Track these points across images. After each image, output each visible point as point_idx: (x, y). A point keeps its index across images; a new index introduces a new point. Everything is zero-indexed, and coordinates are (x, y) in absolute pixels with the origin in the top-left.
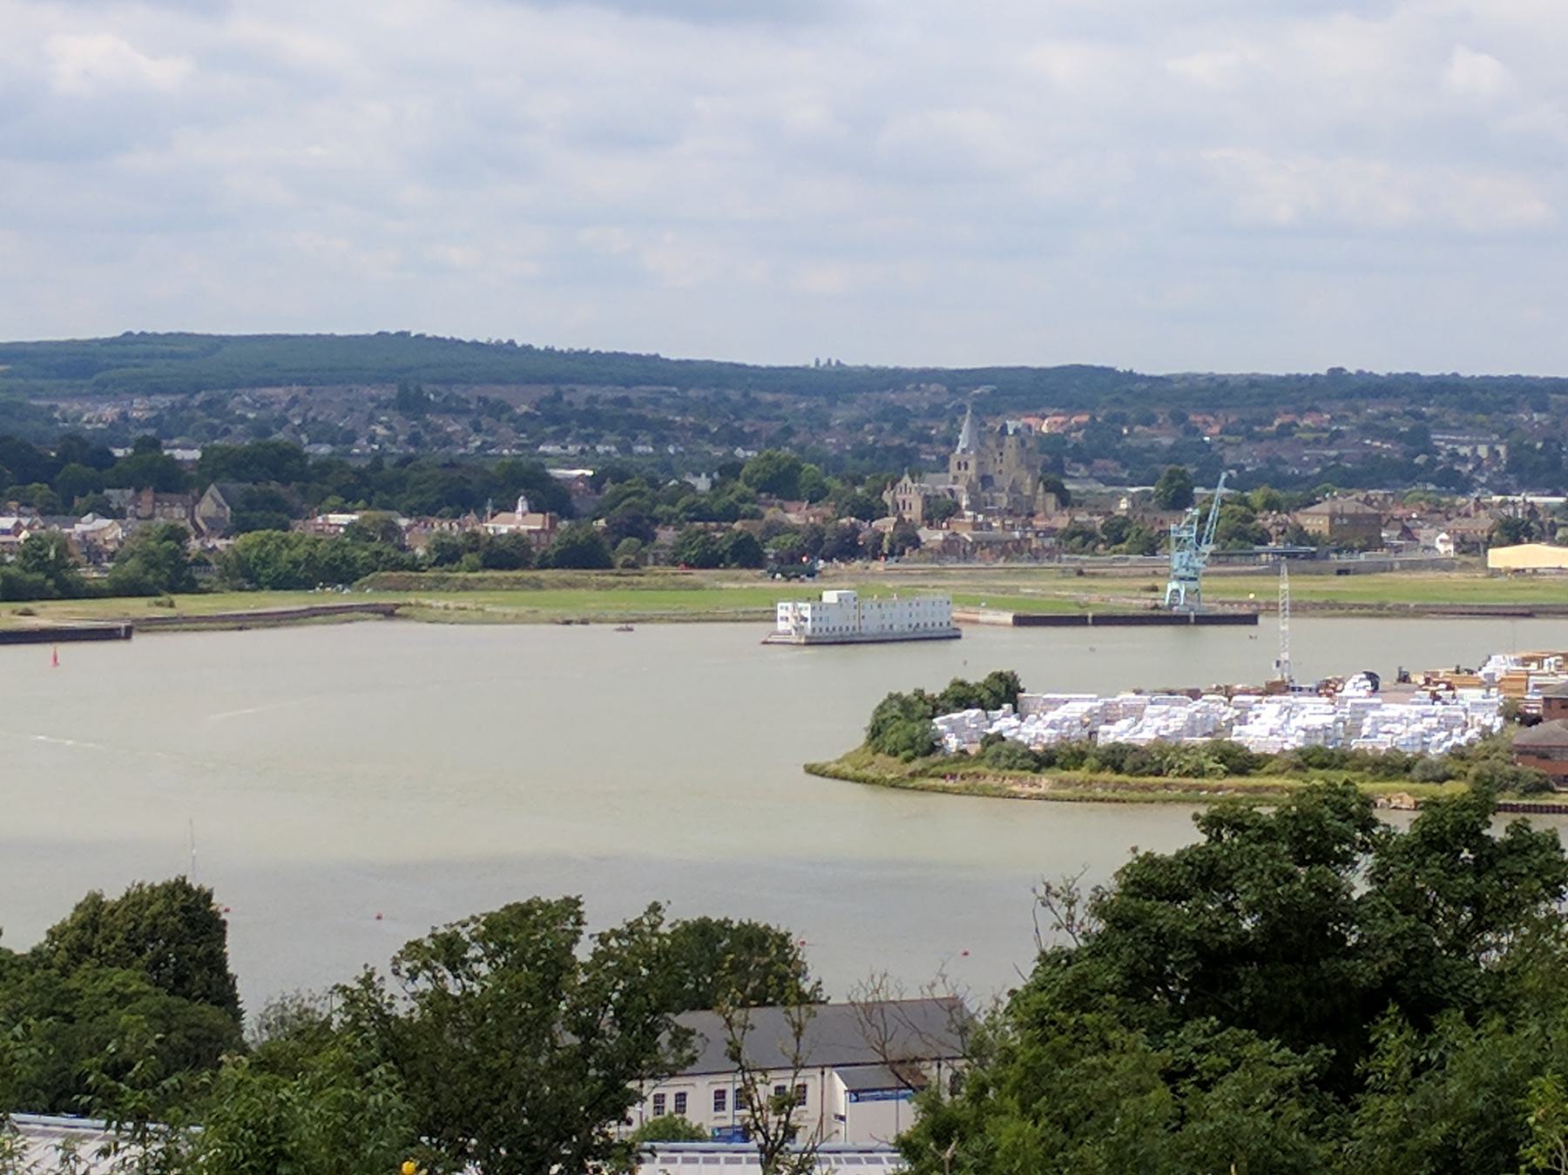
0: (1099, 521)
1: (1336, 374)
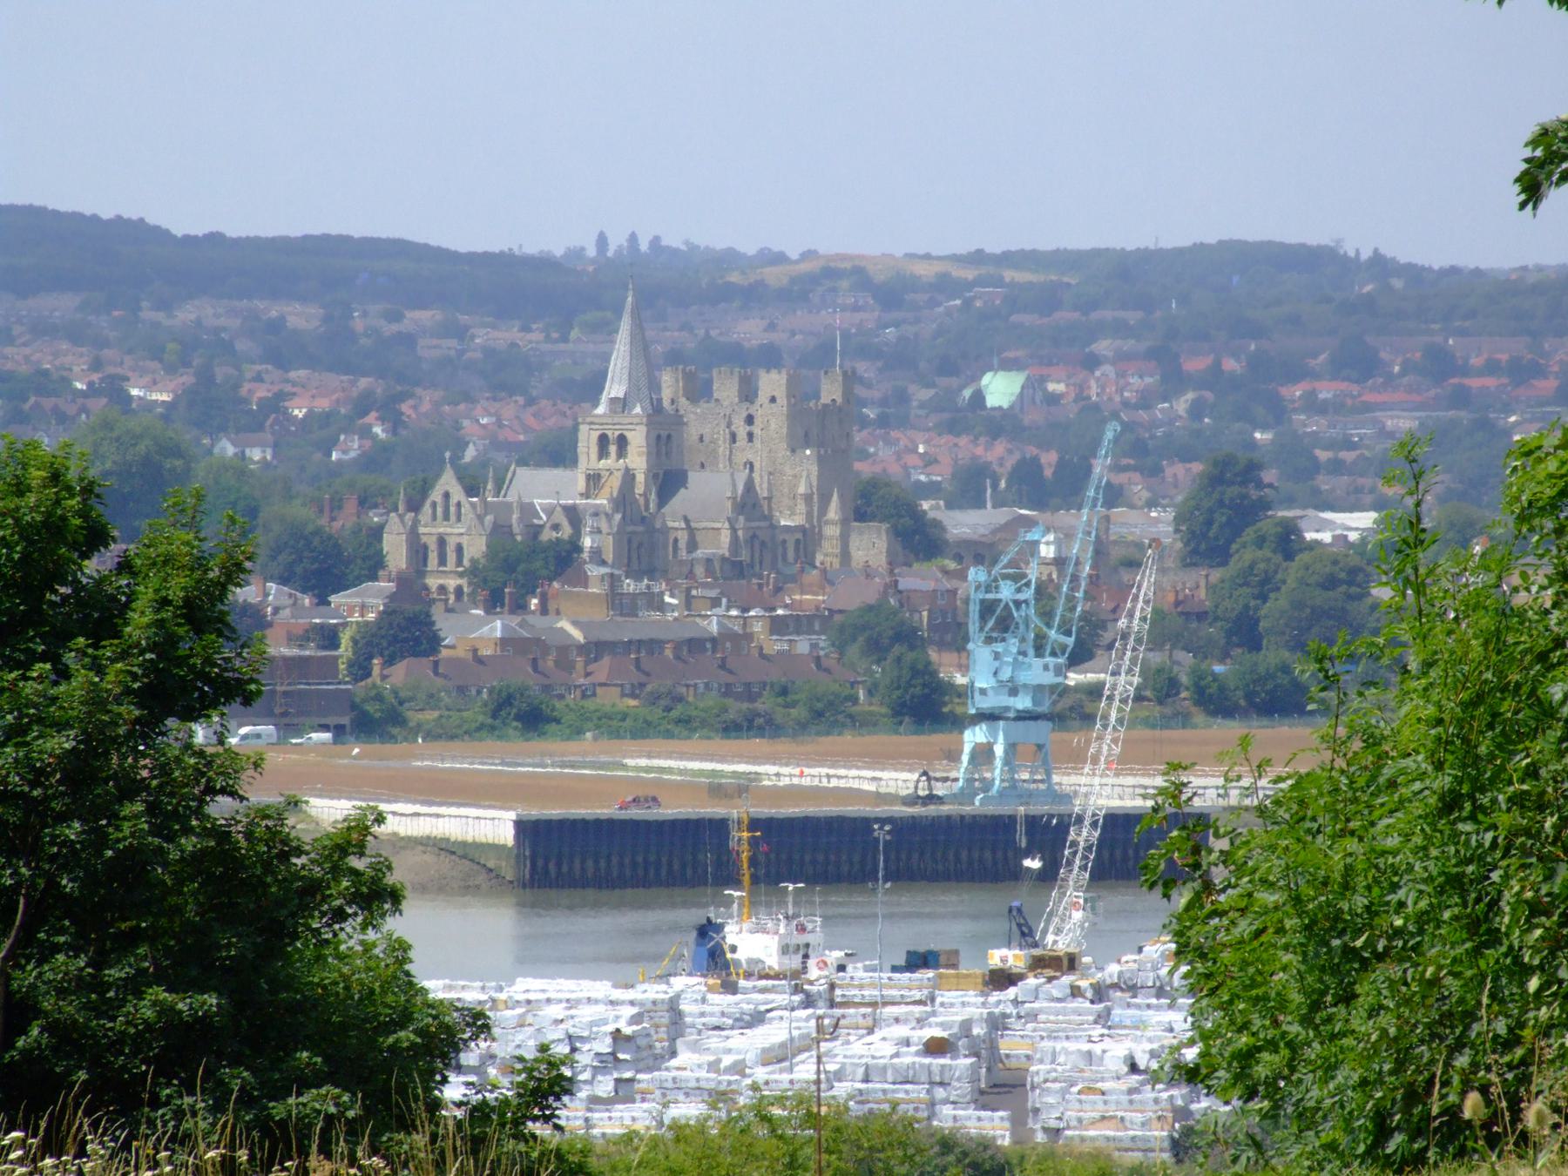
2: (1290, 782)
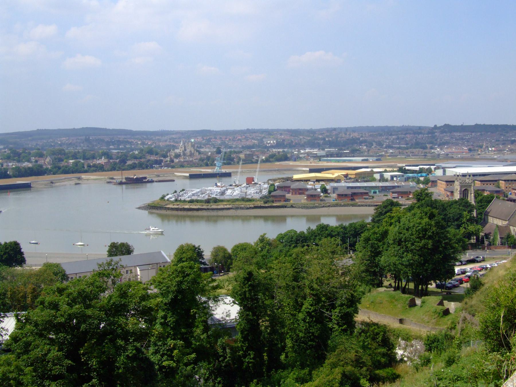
0: (205, 156)
1: (248, 130)
2: (407, 206)
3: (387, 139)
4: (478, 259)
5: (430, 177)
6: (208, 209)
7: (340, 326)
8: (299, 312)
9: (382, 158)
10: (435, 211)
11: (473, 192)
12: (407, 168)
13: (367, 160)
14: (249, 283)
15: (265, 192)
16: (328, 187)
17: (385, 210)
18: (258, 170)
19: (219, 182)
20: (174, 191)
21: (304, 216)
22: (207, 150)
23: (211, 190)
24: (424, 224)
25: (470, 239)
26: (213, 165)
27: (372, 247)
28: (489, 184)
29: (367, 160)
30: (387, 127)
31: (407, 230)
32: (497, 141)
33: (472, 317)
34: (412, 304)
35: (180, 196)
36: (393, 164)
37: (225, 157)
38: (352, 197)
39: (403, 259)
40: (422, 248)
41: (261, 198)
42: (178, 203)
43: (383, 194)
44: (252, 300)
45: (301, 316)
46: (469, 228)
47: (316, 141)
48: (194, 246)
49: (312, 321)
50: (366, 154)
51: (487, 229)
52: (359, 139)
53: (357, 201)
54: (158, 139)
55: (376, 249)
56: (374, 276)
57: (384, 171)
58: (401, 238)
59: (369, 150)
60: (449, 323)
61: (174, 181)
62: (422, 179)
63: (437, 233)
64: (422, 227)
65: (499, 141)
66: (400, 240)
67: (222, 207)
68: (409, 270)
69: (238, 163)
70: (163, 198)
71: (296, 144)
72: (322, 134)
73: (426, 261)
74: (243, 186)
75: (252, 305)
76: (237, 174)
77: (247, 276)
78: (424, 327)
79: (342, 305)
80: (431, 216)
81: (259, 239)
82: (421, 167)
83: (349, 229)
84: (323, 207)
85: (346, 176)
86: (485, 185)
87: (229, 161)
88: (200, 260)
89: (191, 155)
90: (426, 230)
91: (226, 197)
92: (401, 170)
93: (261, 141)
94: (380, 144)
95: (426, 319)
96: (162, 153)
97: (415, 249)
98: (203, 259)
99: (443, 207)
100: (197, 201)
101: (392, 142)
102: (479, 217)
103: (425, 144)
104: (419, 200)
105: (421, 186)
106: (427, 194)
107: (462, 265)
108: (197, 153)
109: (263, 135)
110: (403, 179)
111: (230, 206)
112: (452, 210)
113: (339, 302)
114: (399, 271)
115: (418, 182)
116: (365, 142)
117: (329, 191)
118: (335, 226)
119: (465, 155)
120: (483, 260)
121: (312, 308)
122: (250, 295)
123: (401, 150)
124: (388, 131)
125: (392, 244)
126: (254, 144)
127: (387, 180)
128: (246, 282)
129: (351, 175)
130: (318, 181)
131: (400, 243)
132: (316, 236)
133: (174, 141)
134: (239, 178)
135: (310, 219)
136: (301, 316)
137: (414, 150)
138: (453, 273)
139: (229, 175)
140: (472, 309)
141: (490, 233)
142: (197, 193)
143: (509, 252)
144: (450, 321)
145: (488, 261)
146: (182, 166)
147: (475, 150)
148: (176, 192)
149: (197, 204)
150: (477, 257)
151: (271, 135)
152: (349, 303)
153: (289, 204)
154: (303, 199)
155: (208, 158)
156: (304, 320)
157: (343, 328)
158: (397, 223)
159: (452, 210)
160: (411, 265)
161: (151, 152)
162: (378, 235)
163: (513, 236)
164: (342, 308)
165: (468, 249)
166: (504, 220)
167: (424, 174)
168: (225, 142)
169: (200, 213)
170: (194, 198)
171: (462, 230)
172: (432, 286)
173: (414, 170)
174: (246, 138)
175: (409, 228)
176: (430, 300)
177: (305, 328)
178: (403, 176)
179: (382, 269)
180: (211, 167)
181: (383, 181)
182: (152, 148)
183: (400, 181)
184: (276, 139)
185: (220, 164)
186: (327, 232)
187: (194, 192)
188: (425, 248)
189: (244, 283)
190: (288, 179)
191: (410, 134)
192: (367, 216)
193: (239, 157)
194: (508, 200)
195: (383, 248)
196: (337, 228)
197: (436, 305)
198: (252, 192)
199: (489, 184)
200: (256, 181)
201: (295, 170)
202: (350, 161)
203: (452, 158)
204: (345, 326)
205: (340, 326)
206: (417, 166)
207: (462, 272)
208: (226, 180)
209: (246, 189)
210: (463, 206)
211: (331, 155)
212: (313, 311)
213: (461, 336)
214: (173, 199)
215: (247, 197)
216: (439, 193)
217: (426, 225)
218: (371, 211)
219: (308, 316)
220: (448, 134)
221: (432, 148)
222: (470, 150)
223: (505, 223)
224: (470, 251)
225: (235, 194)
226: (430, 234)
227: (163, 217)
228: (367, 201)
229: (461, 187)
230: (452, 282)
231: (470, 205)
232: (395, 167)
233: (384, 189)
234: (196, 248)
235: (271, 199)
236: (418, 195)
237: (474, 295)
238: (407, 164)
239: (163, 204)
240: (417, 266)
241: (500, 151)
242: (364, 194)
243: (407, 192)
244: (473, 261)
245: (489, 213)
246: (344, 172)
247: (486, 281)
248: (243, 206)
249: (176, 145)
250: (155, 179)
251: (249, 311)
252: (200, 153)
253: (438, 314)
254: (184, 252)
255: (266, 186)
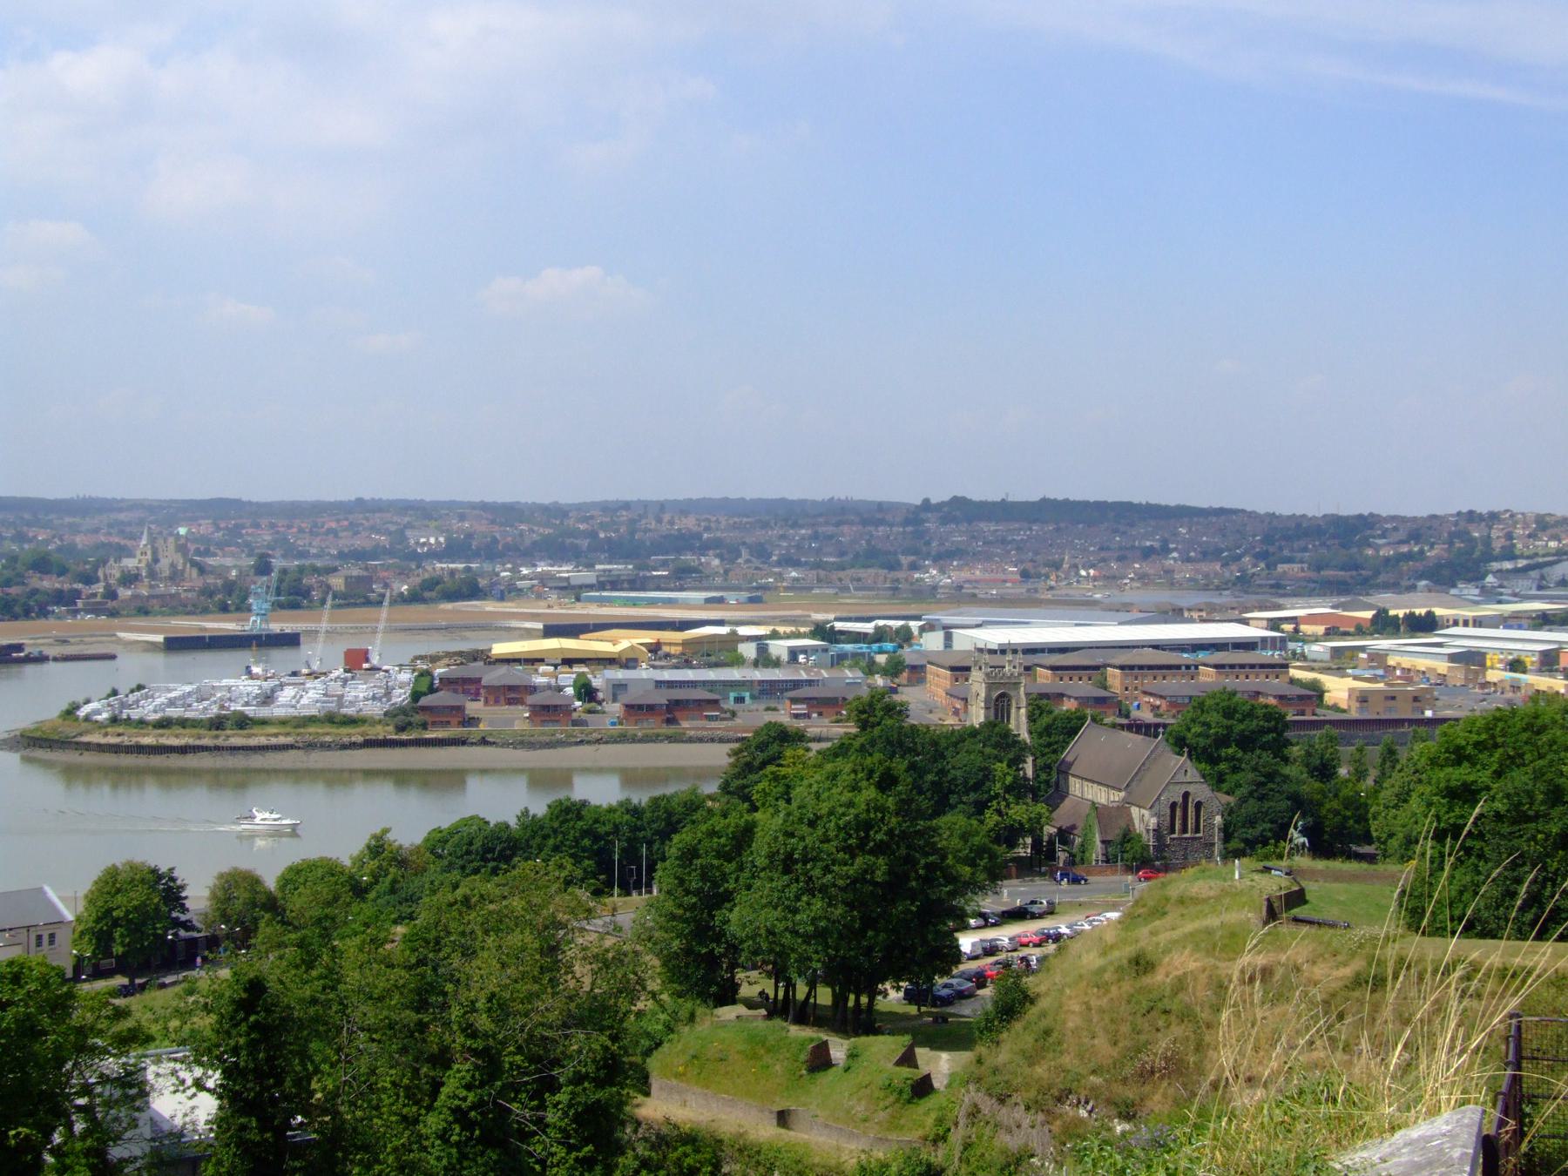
1: (360, 501)
2: (829, 745)
3: (783, 537)
4: (1035, 909)
5: (908, 655)
6: (217, 748)
7: (571, 1148)
8: (430, 1108)
9: (767, 596)
10: (899, 765)
11: (1024, 703)
12: (839, 625)
13: (721, 600)
14: (252, 1018)
15: (401, 696)
16: (597, 682)
17: (761, 756)
18: (381, 626)
19: (257, 663)
20: (109, 691)
21: (521, 771)
22: (228, 562)
23: (229, 689)
24: (863, 807)
25: (1012, 844)
26: (243, 608)
27: (704, 877)
28: (1076, 679)
29: (721, 600)
30: (783, 500)
31: (812, 824)
32: (1101, 549)
33: (996, 1106)
34: (820, 1061)
35: (129, 707)
36: (798, 612)
37: (284, 586)
38: (669, 712)
39: (798, 917)
40: (854, 881)
41: (386, 714)
42: (121, 730)
43: (763, 706)
44: (259, 1075)
45: (433, 1123)
46: (1011, 812)
47: (568, 541)
48: (154, 871)
49: (470, 1139)
50: (718, 581)
51: (1064, 815)
52: (698, 536)
53: (685, 724)
54: (71, 525)
55: (715, 885)
56: (705, 973)
57: (773, 633)
58: (794, 850)
59: (726, 572)
60: (930, 1121)
61: (113, 657)
62: (881, 659)
63: (904, 835)
64: (857, 816)
65: (1108, 549)
66: (789, 856)
67: (263, 741)
68: (817, 952)
69: (323, 602)
70: (70, 712)
71: (507, 547)
72: (586, 520)
73: (868, 922)
74: (332, 676)
75: (259, 1094)
76: (315, 640)
77: (244, 995)
78: (851, 1136)
79: (578, 1079)
80: (887, 782)
81: (368, 847)
82: (881, 623)
83: (648, 815)
84: (581, 742)
85: (654, 648)
86: (1066, 679)
87: (294, 596)
88: (174, 914)
89: (175, 576)
90: (867, 826)
91: (277, 711)
92: (821, 631)
93: (401, 536)
94: (761, 552)
95: (860, 1109)
96: (81, 568)
97: (834, 885)
98: (184, 910)
99: (939, 746)
100: (183, 723)
101: (799, 547)
102: (1043, 776)
103: (895, 553)
104: (864, 726)
105: (880, 681)
106: (890, 709)
107: (986, 925)
108: (195, 572)
109: (407, 519)
110: (827, 658)
111: (289, 740)
112: (962, 758)
113: (563, 1074)
114: (783, 954)
115: (871, 668)
116: (715, 544)
117: (600, 695)
118: (605, 806)
119: (1010, 589)
120: (1050, 911)
121: (471, 1097)
122: (255, 1059)
123: (822, 573)
124: (788, 514)
125: (764, 869)
126: (377, 546)
127: (777, 663)
128: (242, 1015)
129: (670, 644)
130: (569, 662)
131: (788, 864)
132: (545, 837)
133: (122, 532)
134: (322, 652)
135: (539, 779)
136: (433, 1123)
137: (862, 573)
138: (956, 956)
139: (292, 640)
140: (998, 1078)
141: (1073, 827)
142: (184, 696)
143: (1127, 886)
144: (933, 1116)
145: (1065, 913)
146: (144, 612)
147: (1039, 576)
148: (115, 693)
149: (181, 731)
150: (1033, 902)
151: (430, 518)
152: (602, 1073)
153: (474, 732)
154: (518, 718)
155: (229, 587)
156: (443, 1136)
157: (581, 1155)
158: (782, 803)
159: (962, 758)
160: (821, 935)
161: (42, 565)
162: (723, 840)
163: (1140, 836)
164: (579, 1089)
165: (1009, 877)
166: (1114, 788)
167: (889, 646)
168: (286, 539)
169: (190, 761)
170: (174, 712)
171: (991, 818)
172: (892, 997)
173: (859, 633)
174: (354, 529)
175: (818, 818)
176: (874, 1049)
177: (445, 1162)
178: (825, 650)
179: (734, 949)
180: (237, 615)
181: (766, 666)
182: (48, 553)
183: (815, 665)
184: (447, 531)
185: (266, 606)
186: (580, 823)
187: (173, 695)
188: (865, 881)
189: (232, 1019)
190: (475, 656)
191: (851, 523)
192: (703, 774)
193: (329, 587)
194: (1129, 727)
195: (737, 880)
196: (611, 810)
197: (890, 1065)
198: (360, 695)
199: (1076, 679)
200: (375, 660)
201: (497, 629)
202: (670, 603)
203: (973, 599)
204: (590, 1147)
205: (571, 1148)
206: (869, 620)
207: (984, 949)
208: (277, 654)
209: (344, 686)
210: (996, 746)
211: (615, 584)
212: (473, 1107)
213: (964, 1166)
214: (105, 715)
215: (344, 711)
216: (931, 704)
217: (868, 811)
218: (718, 756)
219: (456, 1121)
220: (964, 527)
221: (914, 567)
222: (1025, 575)
223: (1117, 796)
224: (1015, 881)
225: (304, 701)
226: (878, 837)
227: (71, 774)
228: (713, 724)
229: (990, 687)
230: (954, 981)
231: (1016, 742)
232: (804, 624)
233: (769, 690)
234: (160, 877)
235: (417, 718)
236: (863, 712)
237: (1005, 1035)
238: (838, 614)
239: (69, 730)
240: (841, 937)
241: (1111, 579)
242: (706, 703)
243: (836, 699)
244: (1019, 915)
245: (1071, 764)
246: (649, 637)
247: (1043, 988)
248: (328, 739)
249: (129, 543)
250: (51, 652)
251: (249, 1115)
252: (202, 570)
253: (895, 1095)
254: (118, 891)
255: (406, 676)
